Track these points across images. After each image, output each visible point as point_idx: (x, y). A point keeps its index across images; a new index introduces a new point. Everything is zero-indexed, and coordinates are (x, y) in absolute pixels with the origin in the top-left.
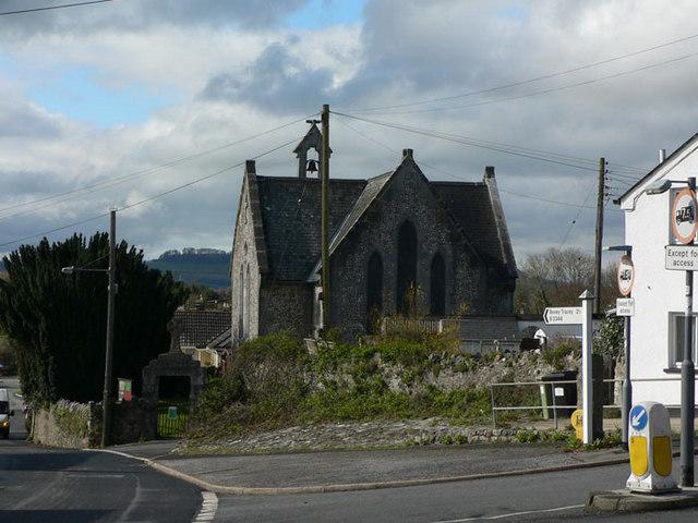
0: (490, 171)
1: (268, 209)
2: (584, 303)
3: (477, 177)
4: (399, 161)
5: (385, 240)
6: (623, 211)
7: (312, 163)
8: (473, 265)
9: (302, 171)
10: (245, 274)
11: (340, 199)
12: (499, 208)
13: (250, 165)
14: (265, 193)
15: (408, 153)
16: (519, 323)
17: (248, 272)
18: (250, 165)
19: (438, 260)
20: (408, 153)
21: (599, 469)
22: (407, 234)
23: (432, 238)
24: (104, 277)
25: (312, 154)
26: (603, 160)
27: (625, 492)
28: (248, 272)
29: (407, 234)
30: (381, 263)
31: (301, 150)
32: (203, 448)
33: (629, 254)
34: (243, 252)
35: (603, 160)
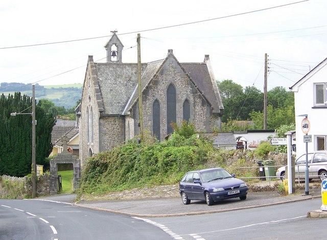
0: (207, 56)
1: (101, 79)
2: (288, 136)
3: (200, 60)
4: (164, 55)
5: (161, 93)
6: (293, 92)
7: (114, 53)
8: (203, 105)
9: (109, 57)
10: (90, 111)
11: (136, 73)
12: (212, 75)
13: (91, 57)
14: (94, 68)
15: (170, 51)
16: (234, 135)
17: (91, 110)
18: (91, 57)
19: (187, 101)
20: (170, 51)
21: (301, 202)
22: (171, 89)
23: (183, 92)
24: (31, 117)
25: (114, 48)
26: (266, 54)
27: (320, 211)
28: (91, 110)
29: (171, 89)
30: (159, 105)
31: (108, 46)
32: (106, 197)
33: (306, 117)
34: (88, 100)
35: (266, 54)
